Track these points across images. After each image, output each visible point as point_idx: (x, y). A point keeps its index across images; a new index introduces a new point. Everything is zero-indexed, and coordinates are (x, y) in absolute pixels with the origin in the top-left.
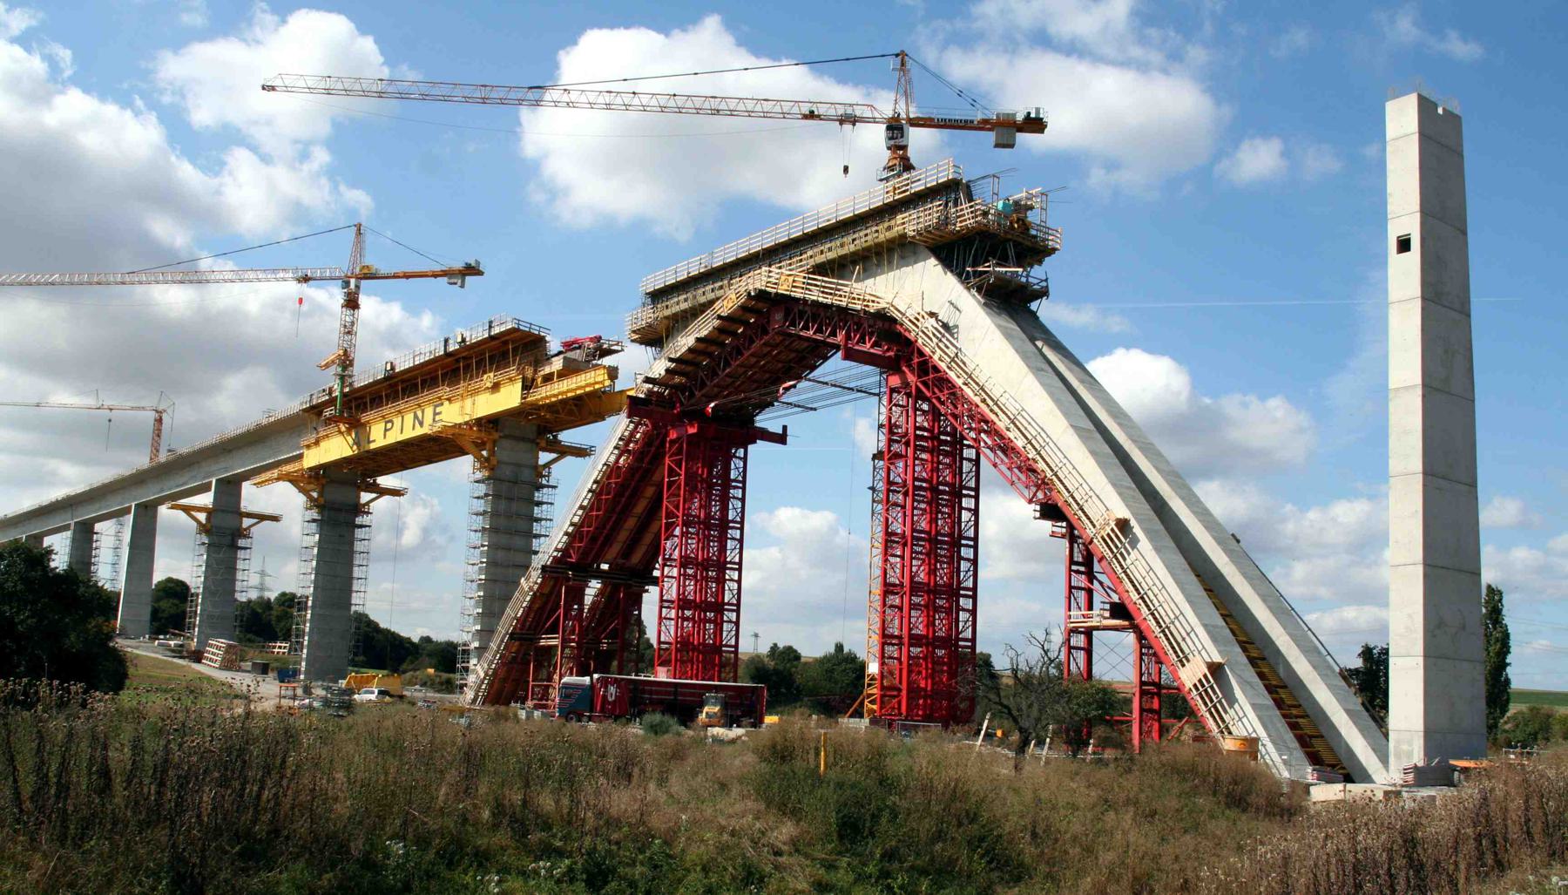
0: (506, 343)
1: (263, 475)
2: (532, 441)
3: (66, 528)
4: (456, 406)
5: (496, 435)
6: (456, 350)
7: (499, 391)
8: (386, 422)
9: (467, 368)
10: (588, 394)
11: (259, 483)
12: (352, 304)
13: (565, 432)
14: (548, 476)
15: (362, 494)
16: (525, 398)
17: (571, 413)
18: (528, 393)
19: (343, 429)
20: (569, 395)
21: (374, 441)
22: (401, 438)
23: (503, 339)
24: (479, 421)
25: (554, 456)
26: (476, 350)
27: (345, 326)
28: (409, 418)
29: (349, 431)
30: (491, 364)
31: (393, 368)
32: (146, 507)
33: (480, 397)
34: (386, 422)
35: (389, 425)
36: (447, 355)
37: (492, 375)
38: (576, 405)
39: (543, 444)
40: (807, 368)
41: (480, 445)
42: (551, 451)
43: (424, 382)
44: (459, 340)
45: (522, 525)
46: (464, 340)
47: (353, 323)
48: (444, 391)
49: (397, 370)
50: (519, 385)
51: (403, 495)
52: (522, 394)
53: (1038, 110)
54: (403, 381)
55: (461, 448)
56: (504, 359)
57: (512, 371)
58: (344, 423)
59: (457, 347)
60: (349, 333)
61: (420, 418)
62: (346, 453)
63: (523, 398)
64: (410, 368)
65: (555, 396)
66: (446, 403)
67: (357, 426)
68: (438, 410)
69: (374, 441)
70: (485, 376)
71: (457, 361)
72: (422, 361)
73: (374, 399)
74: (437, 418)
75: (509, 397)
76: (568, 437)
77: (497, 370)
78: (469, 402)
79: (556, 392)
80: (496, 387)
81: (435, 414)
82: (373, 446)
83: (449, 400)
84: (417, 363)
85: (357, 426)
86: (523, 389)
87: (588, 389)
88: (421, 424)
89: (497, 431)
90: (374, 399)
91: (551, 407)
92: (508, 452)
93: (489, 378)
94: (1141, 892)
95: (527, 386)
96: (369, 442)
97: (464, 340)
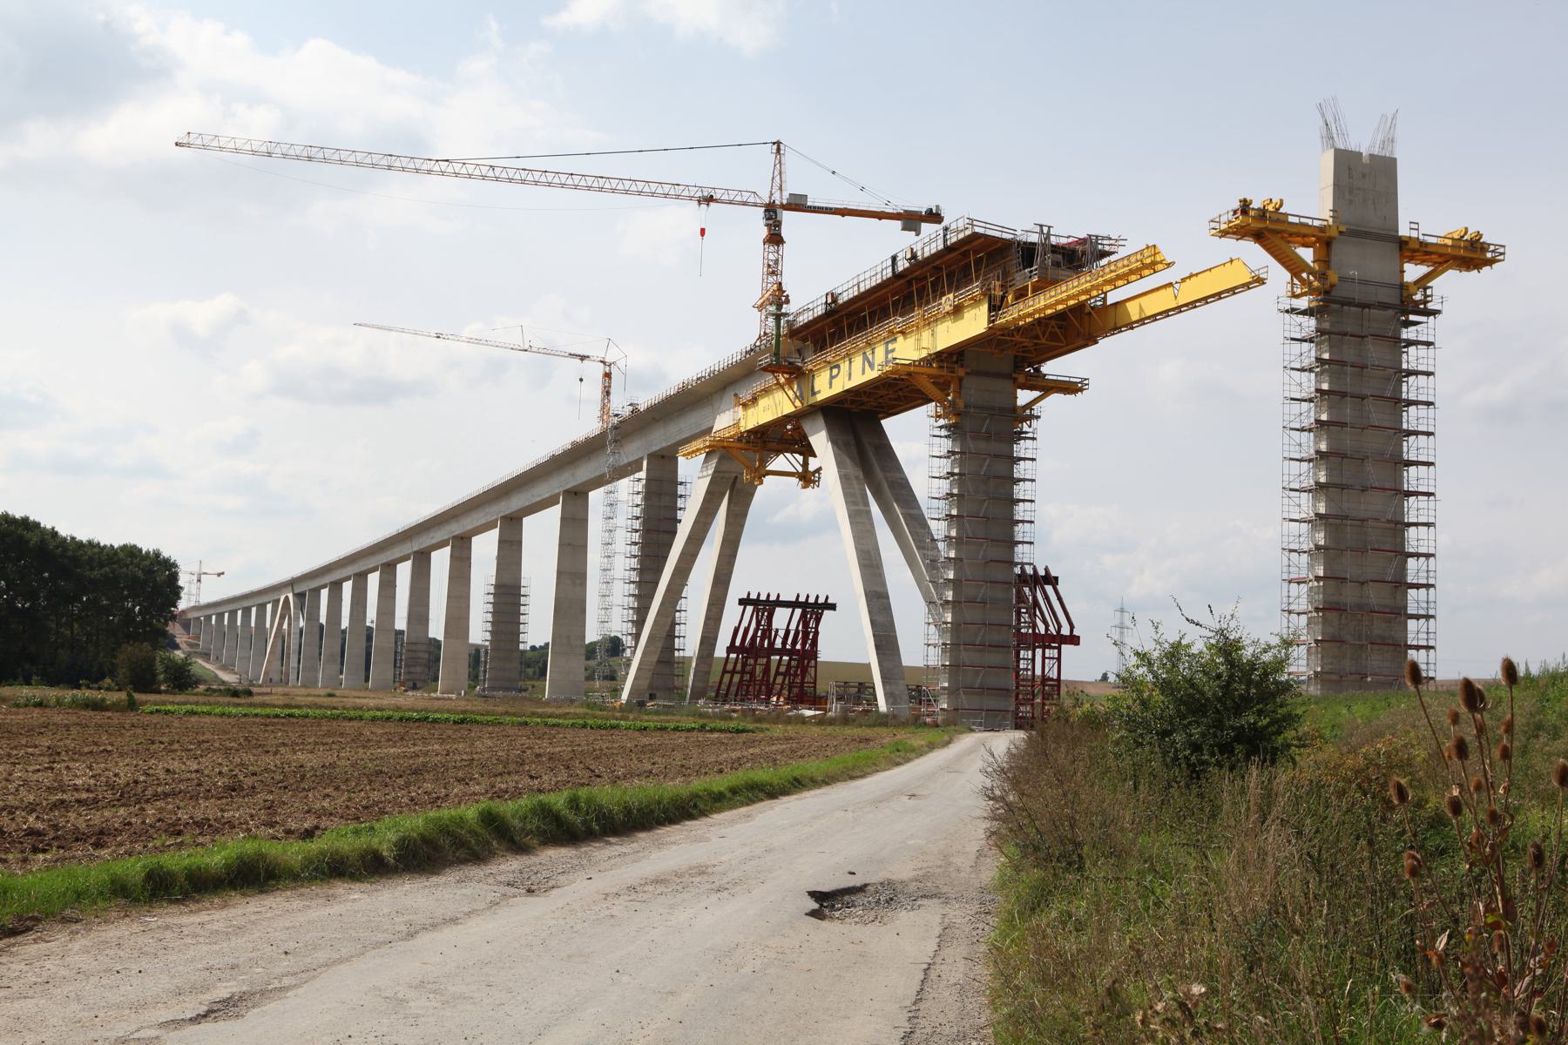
0: (965, 254)
1: (694, 443)
2: (1008, 377)
3: (634, 467)
4: (911, 340)
5: (961, 372)
6: (905, 270)
7: (963, 318)
8: (831, 369)
9: (922, 292)
10: (1072, 309)
11: (689, 454)
12: (777, 238)
13: (1049, 363)
14: (819, 481)
15: (1407, 266)
16: (993, 321)
17: (1053, 337)
18: (996, 315)
19: (782, 380)
20: (1049, 312)
21: (819, 392)
22: (849, 385)
23: (962, 250)
24: (939, 355)
25: (1036, 394)
26: (868, 299)
27: (769, 266)
28: (858, 361)
29: (789, 382)
30: (920, 298)
31: (835, 300)
32: (462, 538)
33: (939, 327)
34: (831, 369)
35: (835, 371)
36: (897, 276)
37: (951, 296)
38: (1060, 327)
39: (1021, 379)
40: (883, 412)
41: (943, 386)
42: (1032, 388)
43: (872, 315)
44: (909, 256)
45: (1348, 412)
46: (914, 256)
47: (776, 262)
48: (898, 321)
49: (840, 302)
50: (985, 307)
51: (1081, 390)
52: (989, 317)
53: (937, 207)
54: (849, 315)
55: (919, 391)
56: (965, 276)
57: (975, 288)
58: (783, 373)
59: (907, 265)
60: (773, 273)
61: (866, 363)
62: (787, 407)
63: (990, 322)
64: (855, 297)
65: (1029, 315)
66: (900, 338)
67: (798, 375)
68: (891, 347)
69: (819, 392)
70: (944, 298)
71: (910, 283)
72: (868, 287)
73: (875, 312)
74: (890, 356)
75: (975, 322)
76: (1053, 368)
77: (958, 289)
78: (926, 334)
79: (1030, 310)
80: (957, 311)
81: (887, 352)
82: (819, 397)
83: (903, 332)
84: (862, 290)
85: (798, 375)
86: (990, 311)
87: (1071, 302)
88: (871, 366)
89: (962, 366)
90: (875, 312)
91: (1025, 331)
92: (977, 390)
93: (948, 301)
94: (1388, 1041)
95: (994, 308)
96: (814, 394)
97: (914, 256)
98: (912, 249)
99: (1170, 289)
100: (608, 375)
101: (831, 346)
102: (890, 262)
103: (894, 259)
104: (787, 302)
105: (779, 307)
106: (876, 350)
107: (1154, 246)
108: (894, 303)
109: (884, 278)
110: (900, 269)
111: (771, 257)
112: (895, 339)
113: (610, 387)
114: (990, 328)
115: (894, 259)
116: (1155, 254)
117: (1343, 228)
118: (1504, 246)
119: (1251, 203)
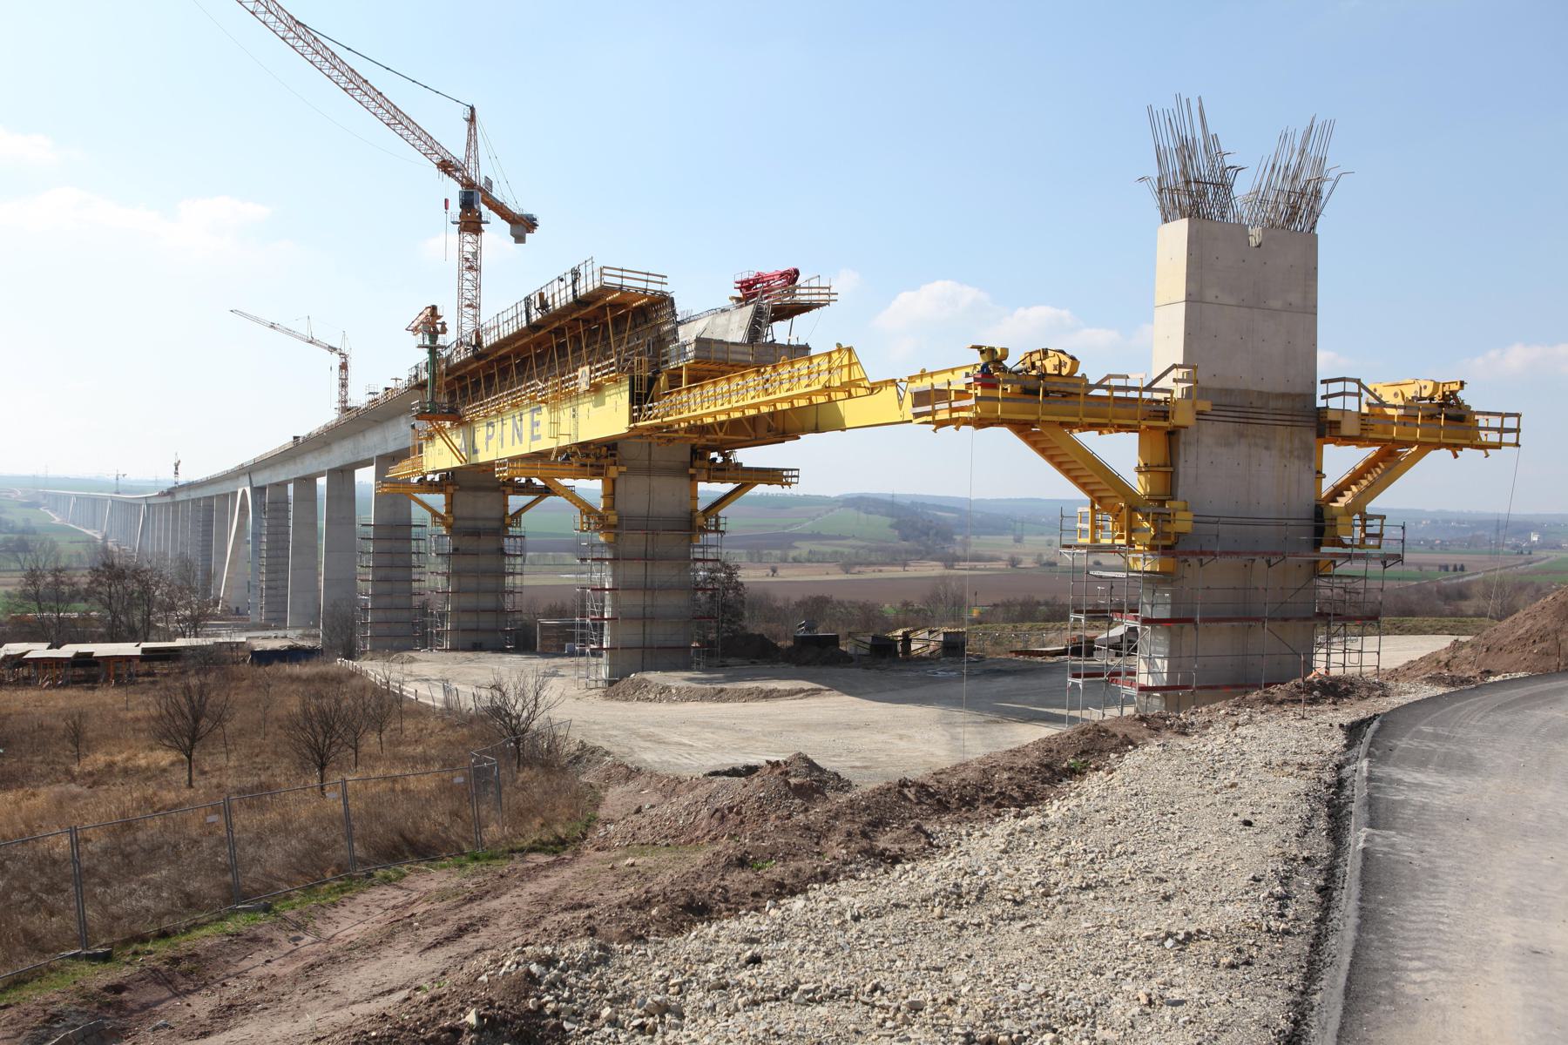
36: (532, 327)
47: (475, 254)
52: (632, 411)
59: (539, 316)
63: (633, 420)
98: (541, 295)
99: (892, 390)
100: (344, 367)
101: (488, 396)
102: (522, 307)
103: (576, 274)
104: (444, 331)
105: (434, 336)
106: (523, 417)
107: (850, 350)
108: (537, 355)
109: (502, 337)
110: (534, 319)
111: (468, 248)
112: (540, 408)
113: (346, 379)
114: (631, 429)
115: (576, 274)
116: (850, 365)
117: (1205, 406)
118: (1518, 415)
119: (1005, 356)
